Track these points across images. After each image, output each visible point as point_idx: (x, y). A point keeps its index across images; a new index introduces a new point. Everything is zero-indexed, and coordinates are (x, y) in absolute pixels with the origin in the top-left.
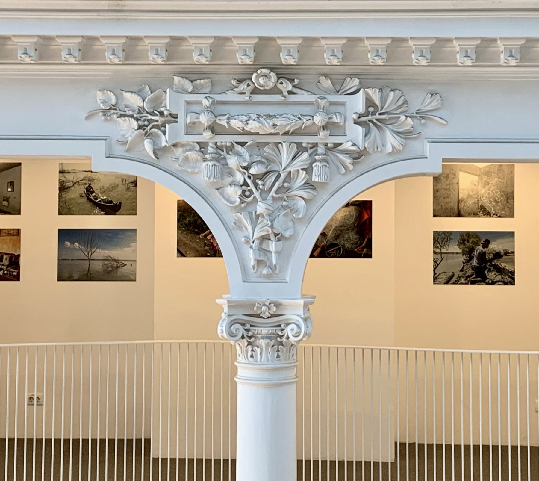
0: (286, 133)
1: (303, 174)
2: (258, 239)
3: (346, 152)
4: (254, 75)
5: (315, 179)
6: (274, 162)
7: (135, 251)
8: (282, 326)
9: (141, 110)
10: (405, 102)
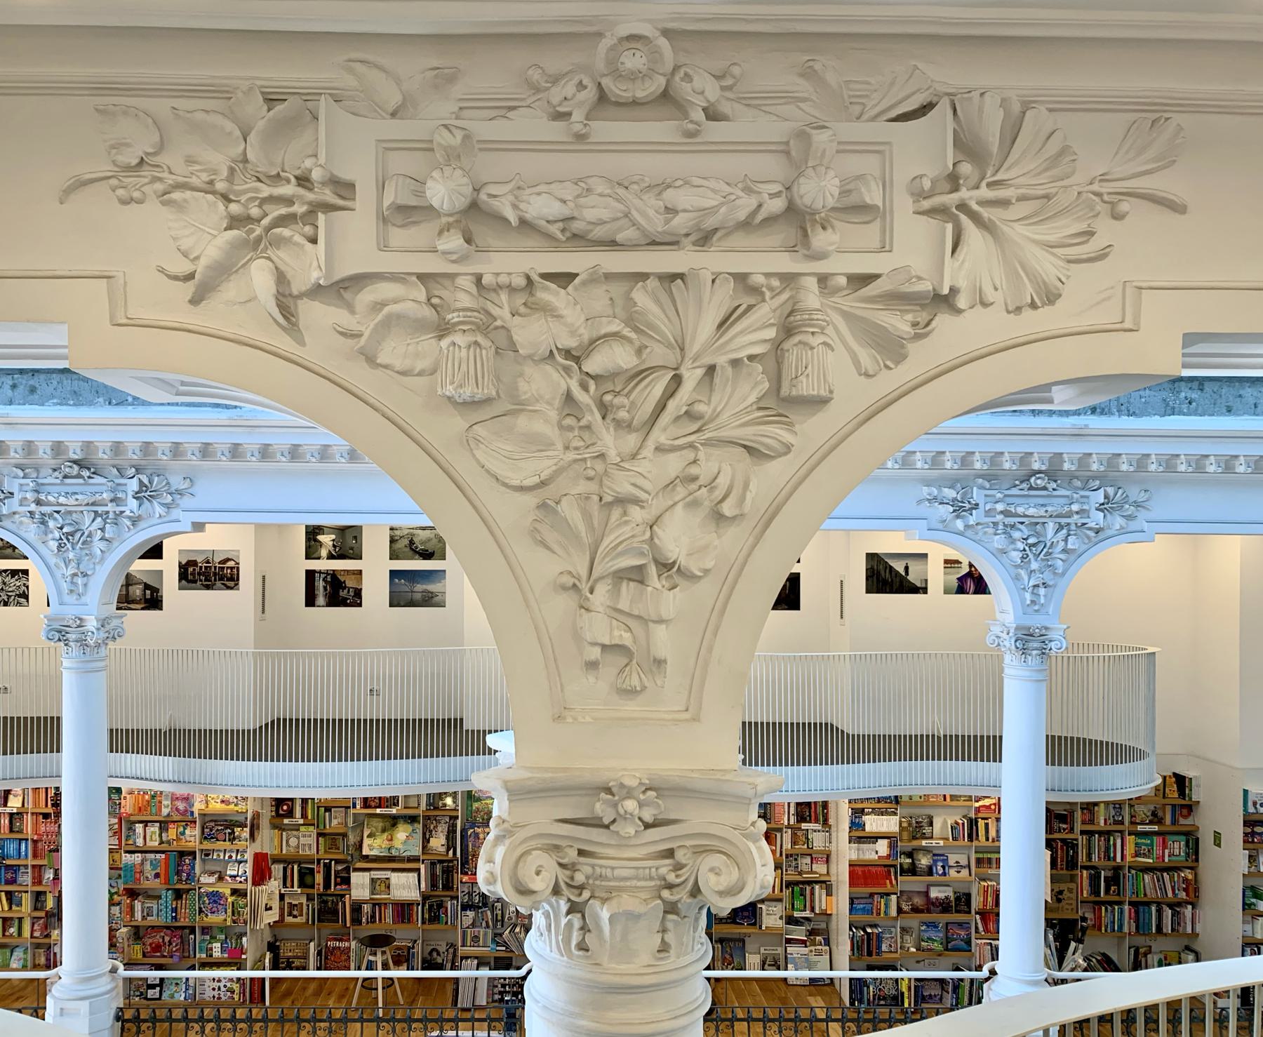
1: (99, 532)
2: (70, 575)
3: (1090, 529)
5: (107, 536)
6: (1042, 536)
7: (445, 586)
9: (955, 500)
10: (168, 483)
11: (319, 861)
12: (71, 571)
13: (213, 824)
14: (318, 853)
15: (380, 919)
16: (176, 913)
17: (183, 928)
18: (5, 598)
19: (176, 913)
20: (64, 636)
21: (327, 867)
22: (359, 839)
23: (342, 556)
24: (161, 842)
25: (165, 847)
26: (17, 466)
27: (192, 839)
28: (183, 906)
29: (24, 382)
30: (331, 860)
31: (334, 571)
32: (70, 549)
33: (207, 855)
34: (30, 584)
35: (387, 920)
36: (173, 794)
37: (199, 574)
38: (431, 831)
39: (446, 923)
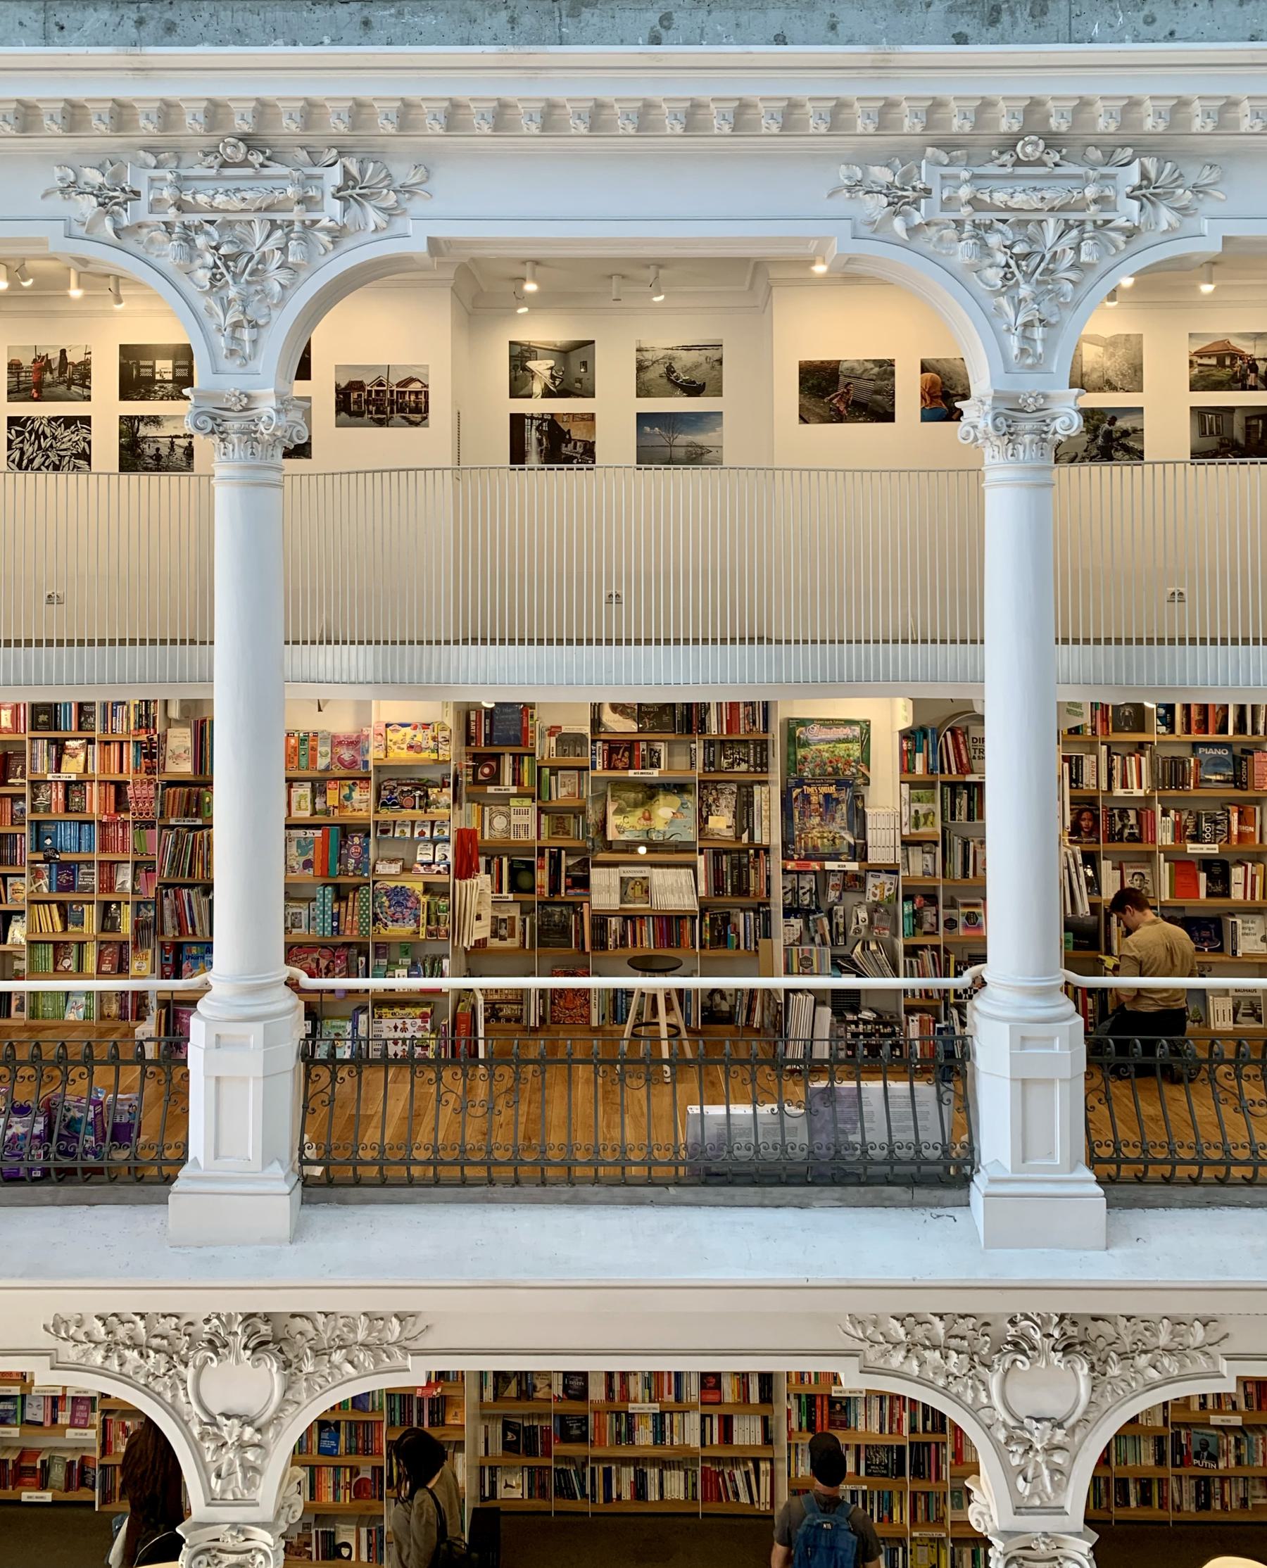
0: (259, 210)
1: (278, 254)
3: (323, 229)
4: (1021, 143)
5: (1084, 258)
7: (721, 436)
10: (389, 175)
11: (541, 851)
12: (233, 316)
13: (394, 783)
14: (539, 838)
15: (634, 942)
16: (338, 921)
17: (348, 945)
18: (56, 460)
19: (338, 921)
20: (219, 425)
21: (556, 860)
22: (600, 816)
23: (564, 393)
24: (314, 813)
25: (320, 819)
26: (147, 149)
27: (363, 806)
28: (350, 909)
29: (157, 15)
30: (560, 849)
31: (552, 415)
32: (231, 282)
33: (385, 832)
34: (93, 438)
35: (645, 943)
36: (334, 737)
37: (367, 402)
38: (709, 806)
39: (738, 947)
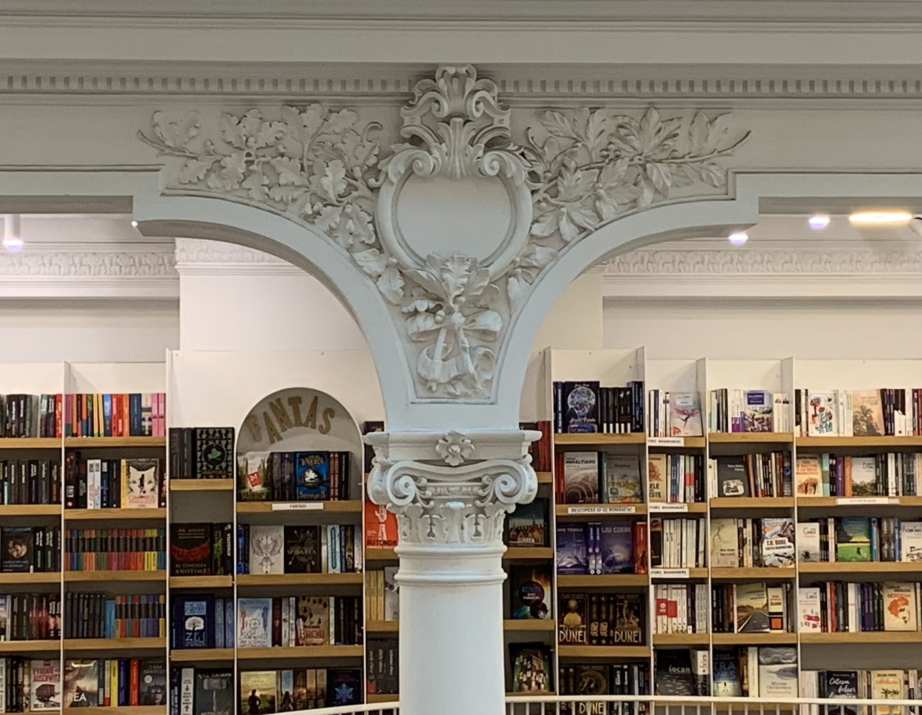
8: (484, 479)
